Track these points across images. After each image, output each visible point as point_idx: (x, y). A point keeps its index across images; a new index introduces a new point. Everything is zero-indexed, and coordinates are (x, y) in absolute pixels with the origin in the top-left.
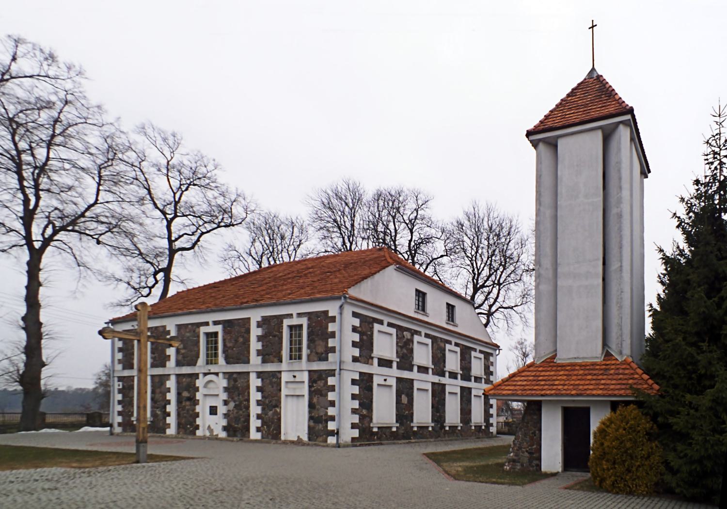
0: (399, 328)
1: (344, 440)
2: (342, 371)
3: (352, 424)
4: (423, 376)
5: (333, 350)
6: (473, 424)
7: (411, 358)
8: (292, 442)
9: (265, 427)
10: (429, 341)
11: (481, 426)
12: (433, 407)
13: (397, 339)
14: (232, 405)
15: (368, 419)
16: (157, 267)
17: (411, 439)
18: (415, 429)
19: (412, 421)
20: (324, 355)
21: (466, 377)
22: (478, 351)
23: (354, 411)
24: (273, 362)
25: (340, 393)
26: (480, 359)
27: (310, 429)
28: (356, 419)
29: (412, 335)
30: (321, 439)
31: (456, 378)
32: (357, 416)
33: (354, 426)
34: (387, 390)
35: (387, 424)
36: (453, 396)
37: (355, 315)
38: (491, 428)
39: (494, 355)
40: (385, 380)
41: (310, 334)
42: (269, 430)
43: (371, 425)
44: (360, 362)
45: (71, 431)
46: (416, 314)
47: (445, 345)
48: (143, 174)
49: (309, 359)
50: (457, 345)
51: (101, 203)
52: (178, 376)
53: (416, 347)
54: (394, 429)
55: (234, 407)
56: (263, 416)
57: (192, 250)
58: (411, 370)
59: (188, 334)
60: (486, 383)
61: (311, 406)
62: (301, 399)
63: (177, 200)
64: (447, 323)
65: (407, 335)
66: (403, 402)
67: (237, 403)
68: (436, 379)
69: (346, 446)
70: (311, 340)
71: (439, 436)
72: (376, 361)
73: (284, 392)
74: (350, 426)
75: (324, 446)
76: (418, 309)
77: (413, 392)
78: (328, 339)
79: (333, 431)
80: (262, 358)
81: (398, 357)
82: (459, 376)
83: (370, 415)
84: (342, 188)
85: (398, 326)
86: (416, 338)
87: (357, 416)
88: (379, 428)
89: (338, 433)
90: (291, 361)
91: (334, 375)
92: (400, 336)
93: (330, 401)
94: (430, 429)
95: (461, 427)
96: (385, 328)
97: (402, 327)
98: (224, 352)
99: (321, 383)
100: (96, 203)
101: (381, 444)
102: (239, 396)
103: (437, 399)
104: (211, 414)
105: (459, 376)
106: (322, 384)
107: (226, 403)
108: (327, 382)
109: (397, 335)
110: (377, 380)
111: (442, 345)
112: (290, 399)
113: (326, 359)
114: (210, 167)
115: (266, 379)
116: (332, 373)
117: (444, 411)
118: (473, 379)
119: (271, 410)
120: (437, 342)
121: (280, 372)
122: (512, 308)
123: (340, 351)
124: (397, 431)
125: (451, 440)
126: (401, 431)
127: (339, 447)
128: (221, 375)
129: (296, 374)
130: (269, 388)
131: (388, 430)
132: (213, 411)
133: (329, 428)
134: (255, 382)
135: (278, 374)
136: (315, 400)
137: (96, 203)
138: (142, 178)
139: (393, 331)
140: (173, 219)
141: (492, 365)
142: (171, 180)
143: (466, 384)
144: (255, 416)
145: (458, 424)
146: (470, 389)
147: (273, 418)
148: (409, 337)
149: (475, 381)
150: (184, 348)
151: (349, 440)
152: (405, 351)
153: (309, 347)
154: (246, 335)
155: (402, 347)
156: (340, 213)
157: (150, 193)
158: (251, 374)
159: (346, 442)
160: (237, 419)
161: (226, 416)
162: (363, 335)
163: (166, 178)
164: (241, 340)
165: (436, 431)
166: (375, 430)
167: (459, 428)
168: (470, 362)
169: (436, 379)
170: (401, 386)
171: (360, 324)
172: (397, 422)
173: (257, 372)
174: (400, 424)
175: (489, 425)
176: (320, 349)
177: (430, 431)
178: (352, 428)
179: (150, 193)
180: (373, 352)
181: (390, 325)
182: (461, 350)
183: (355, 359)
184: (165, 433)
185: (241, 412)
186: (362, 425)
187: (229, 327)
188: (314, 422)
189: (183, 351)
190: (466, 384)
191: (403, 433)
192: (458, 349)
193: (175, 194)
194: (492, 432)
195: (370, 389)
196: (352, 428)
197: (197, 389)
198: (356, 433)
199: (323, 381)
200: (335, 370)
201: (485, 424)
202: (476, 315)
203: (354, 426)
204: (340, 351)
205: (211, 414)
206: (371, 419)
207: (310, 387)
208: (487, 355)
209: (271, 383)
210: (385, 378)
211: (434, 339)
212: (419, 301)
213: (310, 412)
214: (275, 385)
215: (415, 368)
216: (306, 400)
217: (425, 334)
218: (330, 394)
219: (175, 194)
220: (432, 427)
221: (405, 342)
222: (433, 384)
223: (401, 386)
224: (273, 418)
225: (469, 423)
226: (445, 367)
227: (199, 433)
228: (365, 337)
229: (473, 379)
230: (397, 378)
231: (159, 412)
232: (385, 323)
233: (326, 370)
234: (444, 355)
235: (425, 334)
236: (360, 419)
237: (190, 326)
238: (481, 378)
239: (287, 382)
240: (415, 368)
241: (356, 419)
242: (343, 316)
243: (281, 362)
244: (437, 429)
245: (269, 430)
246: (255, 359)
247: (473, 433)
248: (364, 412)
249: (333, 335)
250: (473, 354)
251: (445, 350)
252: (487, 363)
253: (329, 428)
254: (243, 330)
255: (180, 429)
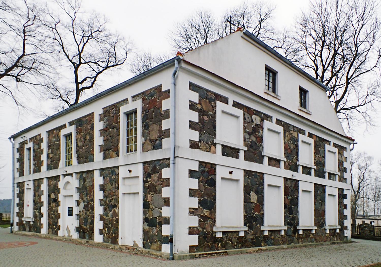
0: (248, 111)
1: (179, 250)
2: (177, 159)
3: (190, 228)
4: (273, 170)
5: (166, 134)
6: (327, 227)
7: (261, 148)
8: (128, 248)
9: (106, 229)
10: (281, 129)
11: (335, 230)
12: (285, 207)
13: (244, 123)
14: (82, 205)
15: (210, 222)
16: (70, 104)
17: (261, 246)
18: (266, 233)
19: (262, 224)
20: (158, 142)
21: (320, 173)
22: (332, 144)
23: (193, 212)
24: (112, 158)
25: (174, 188)
26: (334, 153)
27: (145, 233)
28: (195, 222)
29: (262, 120)
30: (155, 246)
31: (309, 174)
32: (197, 218)
33: (192, 231)
34: (233, 184)
35: (233, 227)
36: (307, 194)
37: (193, 87)
38: (345, 231)
39: (348, 150)
40: (231, 173)
41: (144, 118)
42: (109, 233)
43: (214, 230)
44: (200, 149)
45: (5, 228)
46: (266, 95)
47: (298, 136)
48: (59, 34)
49: (144, 150)
50: (310, 135)
51: (27, 55)
52: (49, 178)
53: (266, 135)
54: (242, 234)
55: (84, 208)
56: (105, 217)
57: (92, 88)
58: (261, 162)
59: (54, 139)
60: (340, 180)
61: (146, 205)
62: (136, 195)
63: (80, 50)
64: (300, 110)
65: (256, 119)
66: (252, 201)
67: (86, 203)
68: (289, 174)
69: (182, 258)
70: (145, 126)
71: (292, 242)
72: (219, 149)
73: (121, 190)
74: (187, 231)
75: (157, 257)
76: (269, 89)
77: (263, 188)
78: (161, 121)
79: (167, 237)
80: (104, 154)
81: (246, 145)
82: (313, 172)
83: (213, 217)
84: (196, 20)
85: (246, 107)
86: (267, 124)
87: (197, 218)
88: (224, 233)
89: (172, 239)
90: (128, 154)
91: (168, 166)
92: (248, 120)
93: (164, 198)
94: (283, 233)
95: (316, 230)
96: (230, 108)
97: (250, 108)
98: (77, 151)
99: (155, 177)
100: (23, 55)
101: (227, 253)
102: (87, 196)
103: (290, 198)
104: (69, 215)
105: (313, 172)
106: (156, 178)
107: (78, 204)
108: (161, 175)
109: (245, 119)
110: (221, 173)
111: (295, 134)
112: (127, 196)
113: (160, 146)
114: (102, 22)
115: (107, 176)
116: (165, 163)
117: (297, 212)
118: (327, 175)
119: (111, 211)
120: (289, 131)
121: (117, 167)
122: (355, 108)
123: (175, 133)
124: (245, 236)
125: (305, 246)
126: (250, 237)
127: (173, 259)
128: (74, 175)
129: (130, 168)
130: (109, 187)
131: (235, 235)
132: (70, 212)
133: (163, 233)
134: (98, 180)
135: (116, 170)
136: (149, 199)
137: (23, 55)
138: (58, 37)
139: (240, 113)
140: (78, 65)
141: (346, 161)
142: (75, 35)
143: (320, 181)
144: (99, 217)
145: (312, 227)
146: (324, 186)
147: (112, 220)
148: (258, 123)
149: (330, 178)
150: (52, 153)
151: (186, 249)
152: (254, 139)
153: (143, 135)
154: (91, 132)
155: (250, 134)
156: (194, 40)
157: (63, 48)
158: (95, 172)
159: (182, 252)
160: (86, 219)
161: (78, 216)
162: (203, 115)
163: (72, 33)
164: (88, 137)
165: (289, 236)
166: (219, 235)
167: (314, 232)
168: (324, 157)
169: (289, 174)
170: (249, 180)
171: (200, 100)
172: (245, 225)
173: (99, 169)
174: (249, 227)
175: (343, 228)
176: (154, 135)
177: (282, 235)
178: (190, 233)
179: (63, 48)
180: (215, 138)
181: (236, 105)
182: (315, 142)
183: (194, 145)
184: (40, 232)
185: (88, 213)
186: (203, 228)
187: (80, 126)
188: (148, 225)
189: (51, 156)
190: (320, 181)
191: (252, 239)
192: (311, 141)
193: (78, 46)
194: (347, 236)
195: (212, 183)
196: (190, 233)
197: (59, 191)
198: (195, 240)
199: (157, 174)
200: (169, 159)
201: (340, 227)
202: (329, 102)
203: (192, 231)
204: (175, 133)
205: (69, 215)
206: (214, 221)
207: (145, 182)
208: (341, 149)
209: (111, 181)
210: (231, 170)
211: (286, 127)
212: (269, 81)
213: (145, 213)
214: (114, 183)
215: (266, 160)
216: (140, 198)
217: (277, 120)
218: (164, 189)
219: (78, 46)
220: (285, 230)
221: (253, 128)
222: (286, 179)
223: (249, 180)
224: (112, 220)
225: (323, 226)
226: (298, 160)
227: (60, 233)
228: (205, 118)
229: (327, 175)
230: (244, 170)
231: (37, 214)
232: (231, 102)
233: (160, 160)
234: (297, 146)
235: (277, 120)
236: (200, 221)
237: (55, 131)
238: (335, 175)
239: (124, 178)
240: (266, 160)
241: (195, 222)
242: (177, 86)
243: (118, 156)
244: (290, 233)
245: (109, 233)
246: (98, 155)
247: (327, 237)
248: (206, 212)
249: (167, 115)
250: (327, 147)
251: (297, 141)
252: (340, 159)
253: (163, 233)
254: (89, 127)
255: (50, 229)
